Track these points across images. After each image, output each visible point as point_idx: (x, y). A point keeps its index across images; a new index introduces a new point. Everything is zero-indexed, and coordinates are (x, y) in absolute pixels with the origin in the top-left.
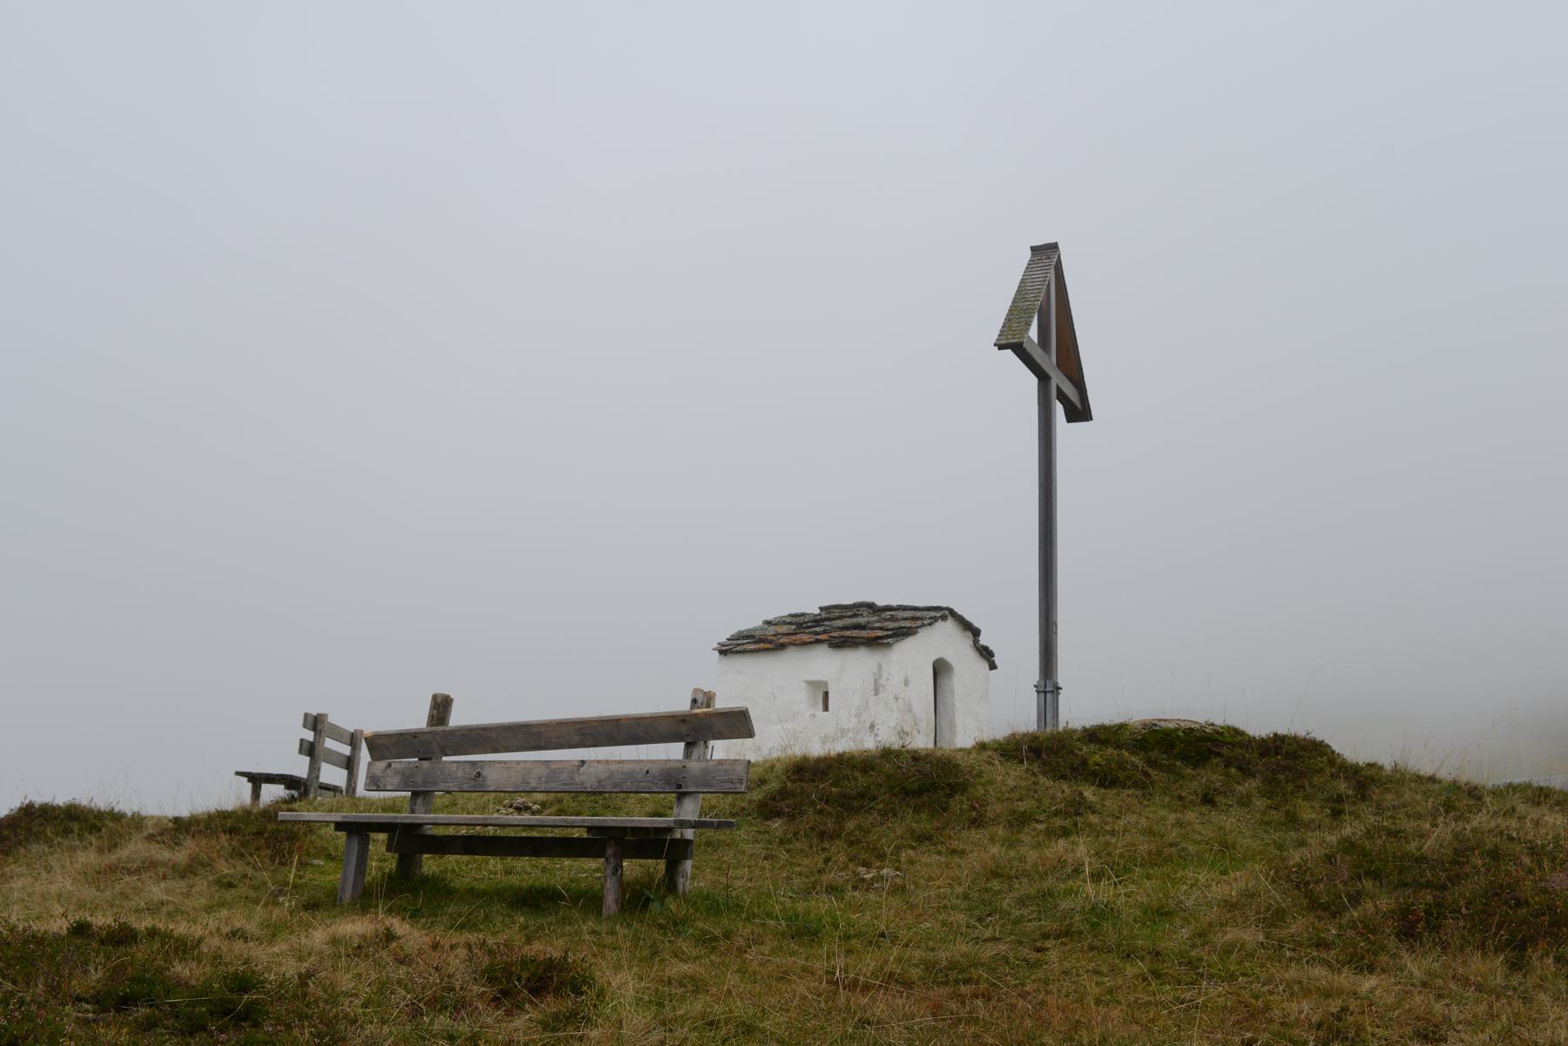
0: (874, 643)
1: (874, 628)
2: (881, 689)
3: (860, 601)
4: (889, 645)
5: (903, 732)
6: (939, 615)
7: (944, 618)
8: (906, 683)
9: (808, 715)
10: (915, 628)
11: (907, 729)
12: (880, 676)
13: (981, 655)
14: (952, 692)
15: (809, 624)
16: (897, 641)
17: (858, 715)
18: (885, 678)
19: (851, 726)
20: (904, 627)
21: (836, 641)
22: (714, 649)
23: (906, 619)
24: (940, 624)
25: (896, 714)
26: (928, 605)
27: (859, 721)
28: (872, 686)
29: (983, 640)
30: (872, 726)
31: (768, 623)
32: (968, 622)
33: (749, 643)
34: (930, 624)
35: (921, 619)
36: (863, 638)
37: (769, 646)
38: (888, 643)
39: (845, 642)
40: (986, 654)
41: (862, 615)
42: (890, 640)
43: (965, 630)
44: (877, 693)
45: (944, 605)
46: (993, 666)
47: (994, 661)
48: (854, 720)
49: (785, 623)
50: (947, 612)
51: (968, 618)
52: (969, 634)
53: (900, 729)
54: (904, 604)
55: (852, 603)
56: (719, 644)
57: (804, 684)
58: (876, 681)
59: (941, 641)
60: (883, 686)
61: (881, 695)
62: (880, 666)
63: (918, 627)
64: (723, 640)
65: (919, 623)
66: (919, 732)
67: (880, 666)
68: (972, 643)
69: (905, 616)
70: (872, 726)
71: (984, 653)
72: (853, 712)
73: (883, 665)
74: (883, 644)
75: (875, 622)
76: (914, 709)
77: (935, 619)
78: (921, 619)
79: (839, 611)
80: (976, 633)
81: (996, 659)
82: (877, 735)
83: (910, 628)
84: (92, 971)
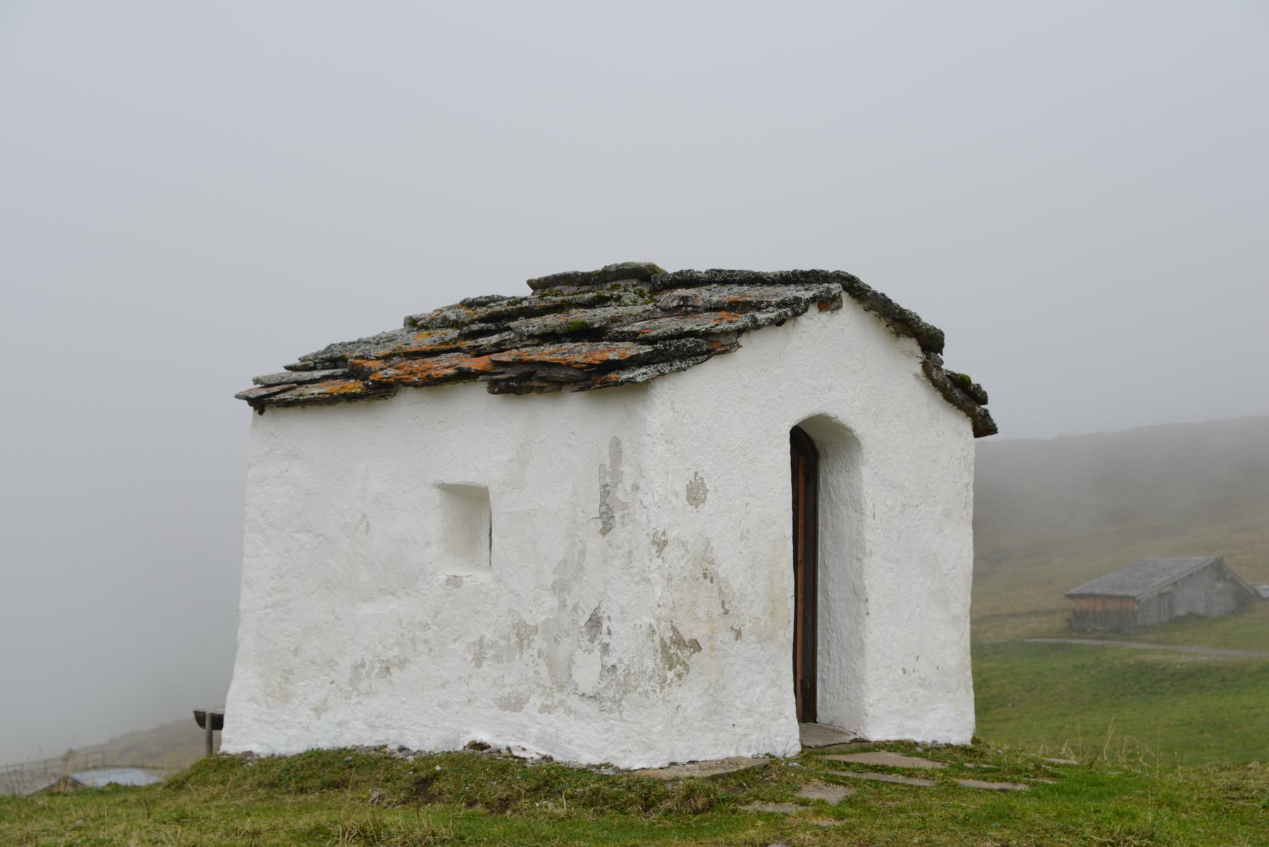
1: (623, 337)
2: (617, 515)
3: (620, 262)
5: (679, 641)
6: (807, 295)
7: (827, 303)
8: (696, 494)
9: (442, 578)
10: (725, 333)
11: (689, 631)
12: (617, 475)
13: (948, 398)
14: (858, 507)
15: (475, 327)
16: (662, 374)
17: (560, 588)
18: (628, 483)
20: (691, 334)
21: (511, 373)
22: (238, 397)
23: (715, 308)
24: (813, 320)
25: (658, 590)
26: (788, 267)
27: (563, 605)
28: (595, 509)
29: (952, 361)
30: (595, 622)
31: (412, 323)
32: (902, 311)
33: (333, 377)
34: (779, 322)
35: (757, 306)
36: (569, 365)
37: (354, 386)
38: (631, 382)
39: (528, 376)
41: (619, 298)
42: (639, 374)
44: (605, 530)
45: (831, 268)
46: (983, 427)
48: (551, 602)
49: (446, 323)
50: (835, 287)
51: (903, 299)
52: (912, 345)
54: (726, 266)
55: (599, 268)
56: (256, 381)
57: (436, 494)
58: (606, 491)
60: (625, 506)
61: (619, 533)
62: (616, 449)
63: (740, 331)
65: (742, 320)
66: (738, 634)
67: (616, 449)
68: (918, 369)
69: (715, 299)
70: (595, 622)
71: (957, 393)
73: (626, 445)
74: (616, 384)
75: (637, 318)
76: (722, 570)
77: (796, 309)
78: (757, 306)
79: (574, 289)
80: (931, 342)
81: (993, 408)
82: (605, 648)
83: (707, 334)
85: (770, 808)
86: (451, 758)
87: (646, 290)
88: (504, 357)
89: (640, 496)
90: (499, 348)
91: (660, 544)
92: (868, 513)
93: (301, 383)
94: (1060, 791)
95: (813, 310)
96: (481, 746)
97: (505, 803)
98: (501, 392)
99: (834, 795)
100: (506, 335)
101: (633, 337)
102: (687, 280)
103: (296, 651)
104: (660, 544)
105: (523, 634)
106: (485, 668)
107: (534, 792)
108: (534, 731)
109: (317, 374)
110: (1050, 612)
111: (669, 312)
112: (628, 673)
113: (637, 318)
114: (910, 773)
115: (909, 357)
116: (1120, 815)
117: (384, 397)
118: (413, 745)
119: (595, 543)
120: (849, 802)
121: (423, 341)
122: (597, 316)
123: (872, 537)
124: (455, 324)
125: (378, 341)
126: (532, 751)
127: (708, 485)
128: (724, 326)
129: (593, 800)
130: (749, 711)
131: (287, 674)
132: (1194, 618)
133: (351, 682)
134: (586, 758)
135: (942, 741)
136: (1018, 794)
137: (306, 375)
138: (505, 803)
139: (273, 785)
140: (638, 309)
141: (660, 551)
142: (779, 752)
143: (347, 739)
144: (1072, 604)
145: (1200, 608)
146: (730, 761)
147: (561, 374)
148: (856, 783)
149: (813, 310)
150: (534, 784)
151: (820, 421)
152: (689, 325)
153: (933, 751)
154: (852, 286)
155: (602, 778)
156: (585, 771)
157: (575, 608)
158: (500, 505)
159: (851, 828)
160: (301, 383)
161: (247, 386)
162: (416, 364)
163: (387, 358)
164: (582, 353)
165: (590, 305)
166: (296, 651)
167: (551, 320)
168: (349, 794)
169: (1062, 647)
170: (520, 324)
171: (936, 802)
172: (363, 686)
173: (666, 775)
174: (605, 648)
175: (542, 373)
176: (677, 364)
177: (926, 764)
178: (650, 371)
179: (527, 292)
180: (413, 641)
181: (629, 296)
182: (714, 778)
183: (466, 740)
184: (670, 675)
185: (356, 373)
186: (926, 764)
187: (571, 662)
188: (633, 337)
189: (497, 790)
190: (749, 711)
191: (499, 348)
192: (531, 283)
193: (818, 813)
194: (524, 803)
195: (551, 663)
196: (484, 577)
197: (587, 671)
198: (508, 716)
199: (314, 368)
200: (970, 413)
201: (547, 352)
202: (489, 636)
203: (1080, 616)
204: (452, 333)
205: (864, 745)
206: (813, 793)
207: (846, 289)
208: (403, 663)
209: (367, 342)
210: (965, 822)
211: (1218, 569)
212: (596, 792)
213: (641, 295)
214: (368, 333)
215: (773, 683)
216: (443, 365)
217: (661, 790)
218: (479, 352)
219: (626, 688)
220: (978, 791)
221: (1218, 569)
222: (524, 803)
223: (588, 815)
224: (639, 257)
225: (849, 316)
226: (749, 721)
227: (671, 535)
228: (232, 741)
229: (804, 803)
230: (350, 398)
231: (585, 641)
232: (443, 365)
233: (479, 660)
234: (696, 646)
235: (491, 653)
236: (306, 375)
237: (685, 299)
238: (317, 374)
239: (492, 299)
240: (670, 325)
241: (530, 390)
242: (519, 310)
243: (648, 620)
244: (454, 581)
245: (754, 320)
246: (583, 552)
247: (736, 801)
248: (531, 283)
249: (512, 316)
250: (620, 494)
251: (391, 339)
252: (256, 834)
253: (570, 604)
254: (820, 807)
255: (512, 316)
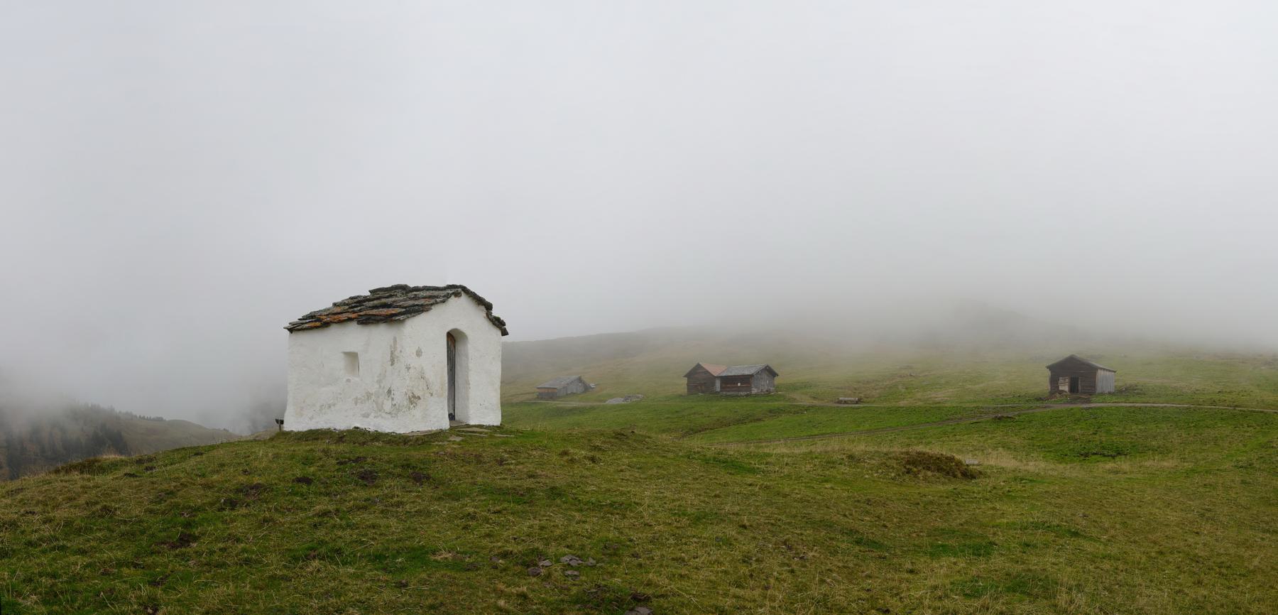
0: (389, 320)
1: (397, 307)
4: (402, 322)
5: (414, 397)
6: (451, 292)
7: (457, 295)
8: (419, 353)
9: (345, 380)
12: (395, 348)
13: (494, 324)
14: (467, 356)
15: (353, 305)
16: (408, 317)
17: (379, 382)
18: (399, 350)
19: (373, 391)
20: (417, 305)
21: (364, 318)
24: (453, 300)
27: (380, 386)
28: (389, 358)
29: (495, 313)
30: (389, 392)
31: (335, 305)
32: (480, 297)
34: (444, 302)
35: (437, 297)
36: (381, 315)
37: (318, 324)
38: (399, 320)
39: (369, 319)
40: (499, 323)
42: (401, 317)
43: (479, 304)
44: (392, 365)
46: (504, 333)
47: (505, 329)
50: (460, 290)
52: (483, 308)
53: (411, 395)
55: (390, 286)
57: (342, 355)
58: (392, 353)
59: (457, 314)
60: (398, 357)
63: (432, 305)
64: (295, 320)
66: (432, 395)
68: (485, 315)
70: (389, 392)
71: (496, 322)
72: (376, 379)
74: (396, 320)
75: (401, 301)
76: (427, 376)
77: (448, 296)
78: (437, 297)
80: (489, 307)
81: (507, 327)
82: (393, 399)
83: (422, 305)
84: (100, 464)
85: (440, 443)
86: (348, 431)
87: (404, 292)
88: (361, 313)
89: (402, 354)
90: (360, 311)
91: (408, 368)
92: (470, 358)
93: (303, 324)
94: (523, 436)
95: (453, 297)
96: (358, 428)
97: (364, 443)
98: (361, 324)
99: (458, 439)
100: (362, 307)
101: (400, 307)
102: (417, 289)
103: (304, 402)
104: (408, 368)
105: (369, 396)
106: (358, 406)
107: (372, 440)
108: (372, 423)
109: (307, 321)
110: (533, 393)
111: (411, 299)
112: (399, 406)
113: (401, 301)
114: (481, 433)
115: (481, 312)
116: (538, 442)
117: (327, 327)
118: (338, 428)
119: (389, 368)
120: (462, 441)
121: (338, 310)
122: (389, 301)
123: (471, 365)
124: (347, 305)
125: (325, 310)
126: (372, 429)
127: (423, 351)
128: (427, 303)
129: (389, 442)
130: (435, 417)
131: (302, 409)
132: (573, 394)
133: (320, 410)
134: (387, 431)
135: (491, 424)
136: (511, 438)
137: (304, 321)
138: (364, 443)
139: (299, 439)
140: (402, 298)
141: (408, 370)
142: (443, 428)
143: (319, 426)
144: (538, 390)
145: (575, 391)
146: (430, 431)
147: (379, 318)
148: (465, 436)
149: (453, 297)
150: (372, 438)
151: (455, 330)
152: (416, 303)
153: (488, 427)
154: (465, 289)
155: (392, 436)
156: (387, 434)
157: (384, 387)
158: (361, 358)
159: (462, 447)
160: (303, 324)
161: (287, 325)
162: (336, 317)
163: (327, 315)
164: (384, 311)
165: (387, 297)
166: (304, 402)
167: (376, 302)
168: (319, 441)
169: (535, 403)
170: (367, 304)
171: (487, 440)
172: (323, 411)
173: (410, 435)
174: (393, 399)
175: (373, 318)
176: (413, 314)
177: (486, 431)
178: (405, 316)
179: (369, 294)
180: (337, 398)
181: (399, 294)
182: (424, 436)
183: (353, 426)
184: (412, 406)
185: (319, 320)
186: (486, 431)
187: (383, 403)
188: (400, 307)
189: (362, 439)
190: (435, 417)
191: (360, 311)
192: (370, 291)
193: (453, 444)
194: (369, 443)
195: (377, 403)
196: (357, 379)
197: (387, 406)
198: (365, 419)
199: (306, 319)
200: (501, 329)
201: (375, 312)
202: (359, 396)
203: (540, 394)
204: (347, 307)
205: (468, 426)
206: (452, 439)
207: (463, 290)
208: (334, 405)
209: (322, 311)
210: (495, 445)
211: (580, 380)
212: (390, 440)
213: (403, 294)
214: (322, 308)
215: (442, 409)
216: (344, 317)
217: (409, 439)
218: (354, 312)
219: (399, 410)
220: (500, 437)
221: (580, 380)
222: (369, 443)
223: (388, 446)
224: (403, 283)
225: (464, 298)
226: (435, 420)
227: (411, 366)
228: (287, 427)
229: (450, 441)
230: (317, 327)
231: (387, 397)
232: (344, 317)
233: (356, 403)
234: (419, 398)
235: (359, 401)
236: (304, 321)
237: (416, 295)
238: (307, 321)
239: (358, 296)
240: (411, 303)
241: (369, 323)
242: (366, 299)
243: (405, 390)
244: (348, 381)
245: (436, 301)
246: (386, 371)
247: (431, 442)
248: (370, 291)
249: (364, 301)
250: (397, 353)
251: (329, 310)
252: (294, 451)
253: (382, 386)
254: (454, 442)
255: (364, 301)
